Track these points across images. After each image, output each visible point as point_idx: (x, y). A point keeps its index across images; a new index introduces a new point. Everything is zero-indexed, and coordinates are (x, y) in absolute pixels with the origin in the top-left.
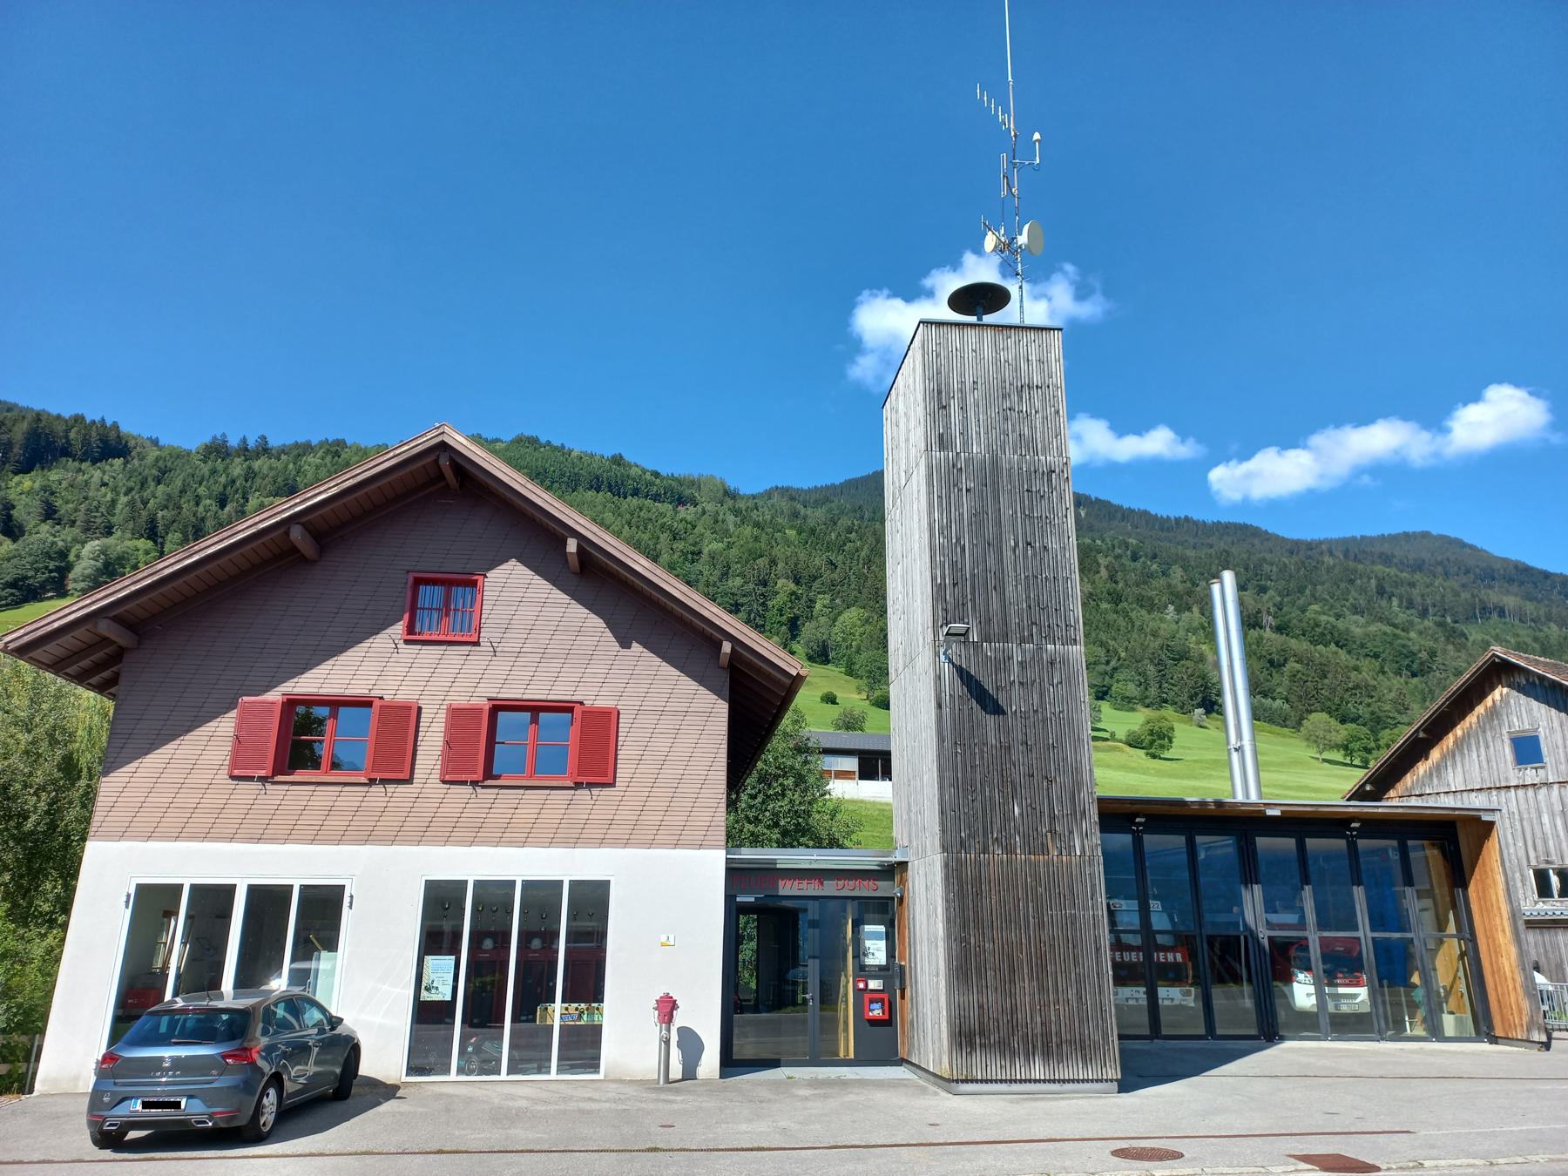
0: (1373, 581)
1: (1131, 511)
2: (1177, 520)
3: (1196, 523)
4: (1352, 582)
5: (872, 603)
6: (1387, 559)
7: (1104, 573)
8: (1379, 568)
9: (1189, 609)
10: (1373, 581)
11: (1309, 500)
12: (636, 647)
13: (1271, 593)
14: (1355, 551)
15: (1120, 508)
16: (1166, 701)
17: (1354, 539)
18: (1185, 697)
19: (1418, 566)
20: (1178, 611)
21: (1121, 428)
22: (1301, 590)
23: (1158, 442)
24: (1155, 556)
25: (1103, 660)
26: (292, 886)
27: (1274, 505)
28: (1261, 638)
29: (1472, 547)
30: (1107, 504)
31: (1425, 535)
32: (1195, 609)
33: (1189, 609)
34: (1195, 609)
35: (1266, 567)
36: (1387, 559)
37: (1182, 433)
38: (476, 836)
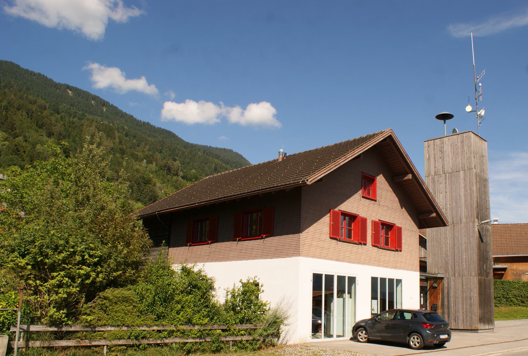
0: (214, 165)
1: (126, 114)
2: (144, 123)
3: (151, 126)
4: (206, 163)
5: (10, 131)
6: (218, 157)
7: (117, 140)
8: (216, 160)
9: (152, 163)
10: (214, 165)
11: (198, 127)
12: (404, 209)
13: (178, 162)
14: (208, 151)
15: (121, 111)
16: (139, 200)
17: (207, 146)
18: (147, 199)
19: (227, 163)
20: (148, 163)
21: (130, 75)
22: (189, 163)
23: (140, 84)
24: (135, 137)
25: (116, 178)
26: (333, 276)
27: (182, 125)
28: (177, 180)
29: (245, 159)
30: (116, 108)
31: (231, 151)
32: (154, 164)
33: (152, 163)
34: (154, 164)
35: (177, 151)
36: (218, 157)
37: (150, 83)
38: (386, 265)
